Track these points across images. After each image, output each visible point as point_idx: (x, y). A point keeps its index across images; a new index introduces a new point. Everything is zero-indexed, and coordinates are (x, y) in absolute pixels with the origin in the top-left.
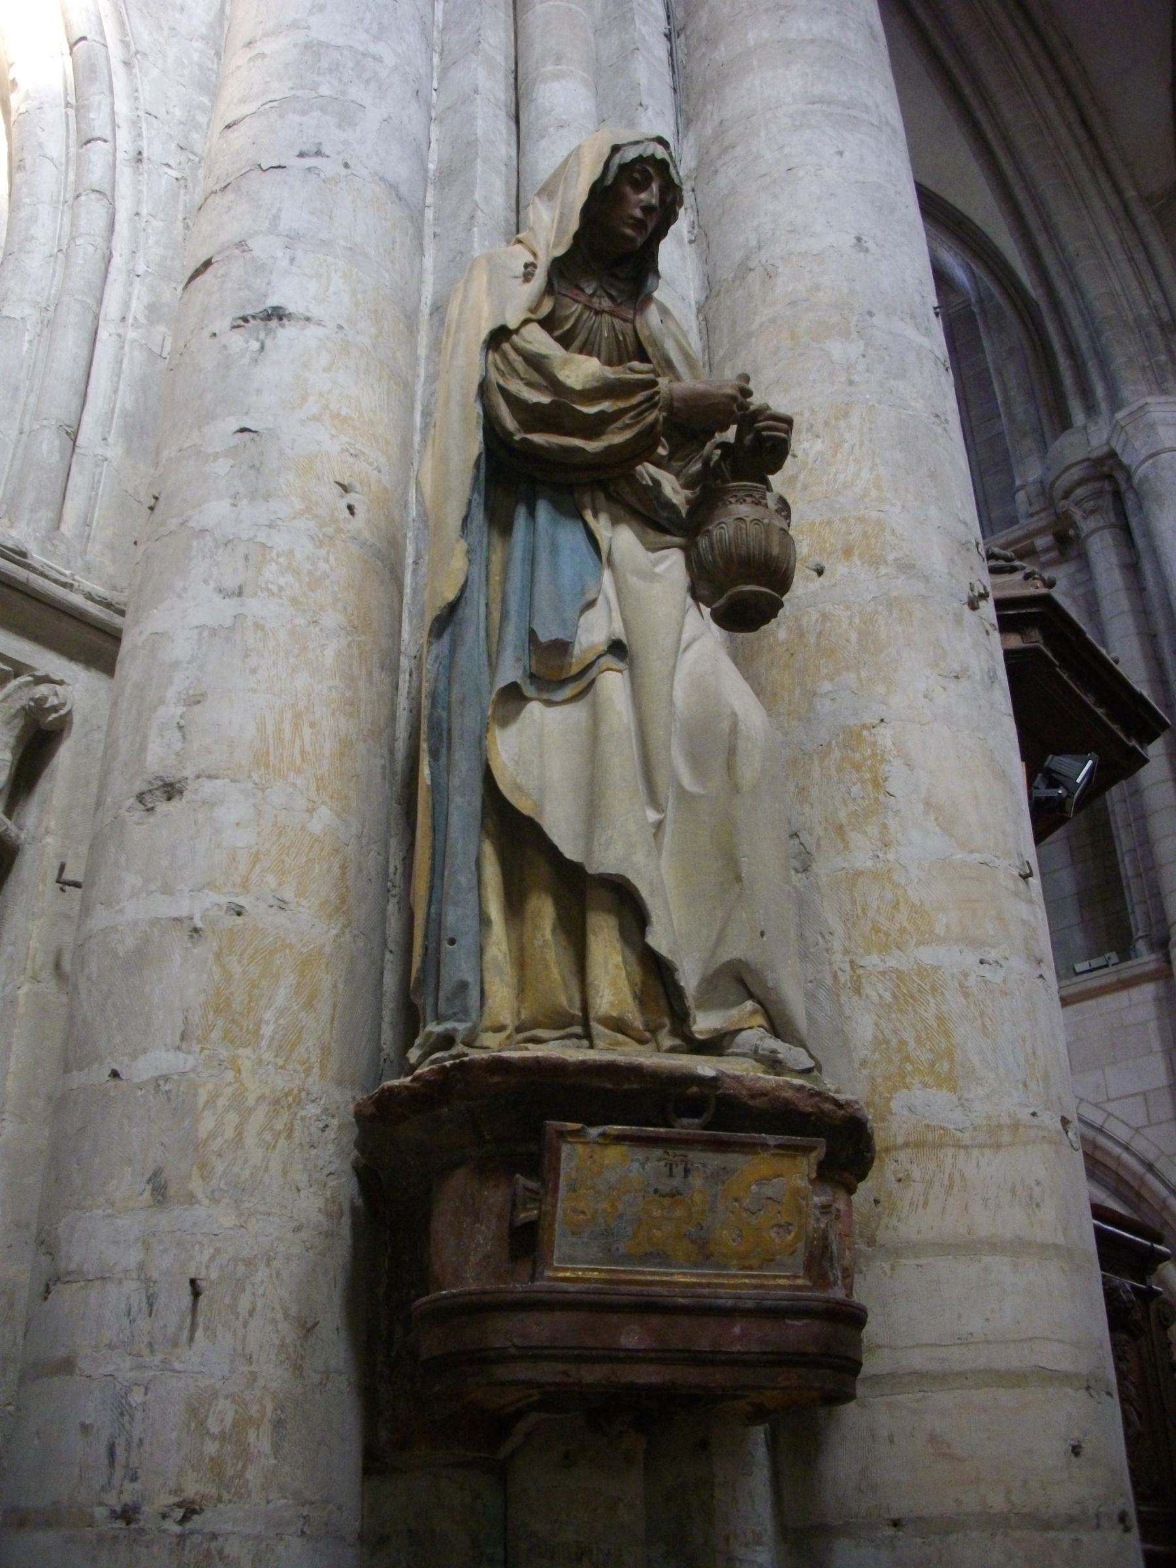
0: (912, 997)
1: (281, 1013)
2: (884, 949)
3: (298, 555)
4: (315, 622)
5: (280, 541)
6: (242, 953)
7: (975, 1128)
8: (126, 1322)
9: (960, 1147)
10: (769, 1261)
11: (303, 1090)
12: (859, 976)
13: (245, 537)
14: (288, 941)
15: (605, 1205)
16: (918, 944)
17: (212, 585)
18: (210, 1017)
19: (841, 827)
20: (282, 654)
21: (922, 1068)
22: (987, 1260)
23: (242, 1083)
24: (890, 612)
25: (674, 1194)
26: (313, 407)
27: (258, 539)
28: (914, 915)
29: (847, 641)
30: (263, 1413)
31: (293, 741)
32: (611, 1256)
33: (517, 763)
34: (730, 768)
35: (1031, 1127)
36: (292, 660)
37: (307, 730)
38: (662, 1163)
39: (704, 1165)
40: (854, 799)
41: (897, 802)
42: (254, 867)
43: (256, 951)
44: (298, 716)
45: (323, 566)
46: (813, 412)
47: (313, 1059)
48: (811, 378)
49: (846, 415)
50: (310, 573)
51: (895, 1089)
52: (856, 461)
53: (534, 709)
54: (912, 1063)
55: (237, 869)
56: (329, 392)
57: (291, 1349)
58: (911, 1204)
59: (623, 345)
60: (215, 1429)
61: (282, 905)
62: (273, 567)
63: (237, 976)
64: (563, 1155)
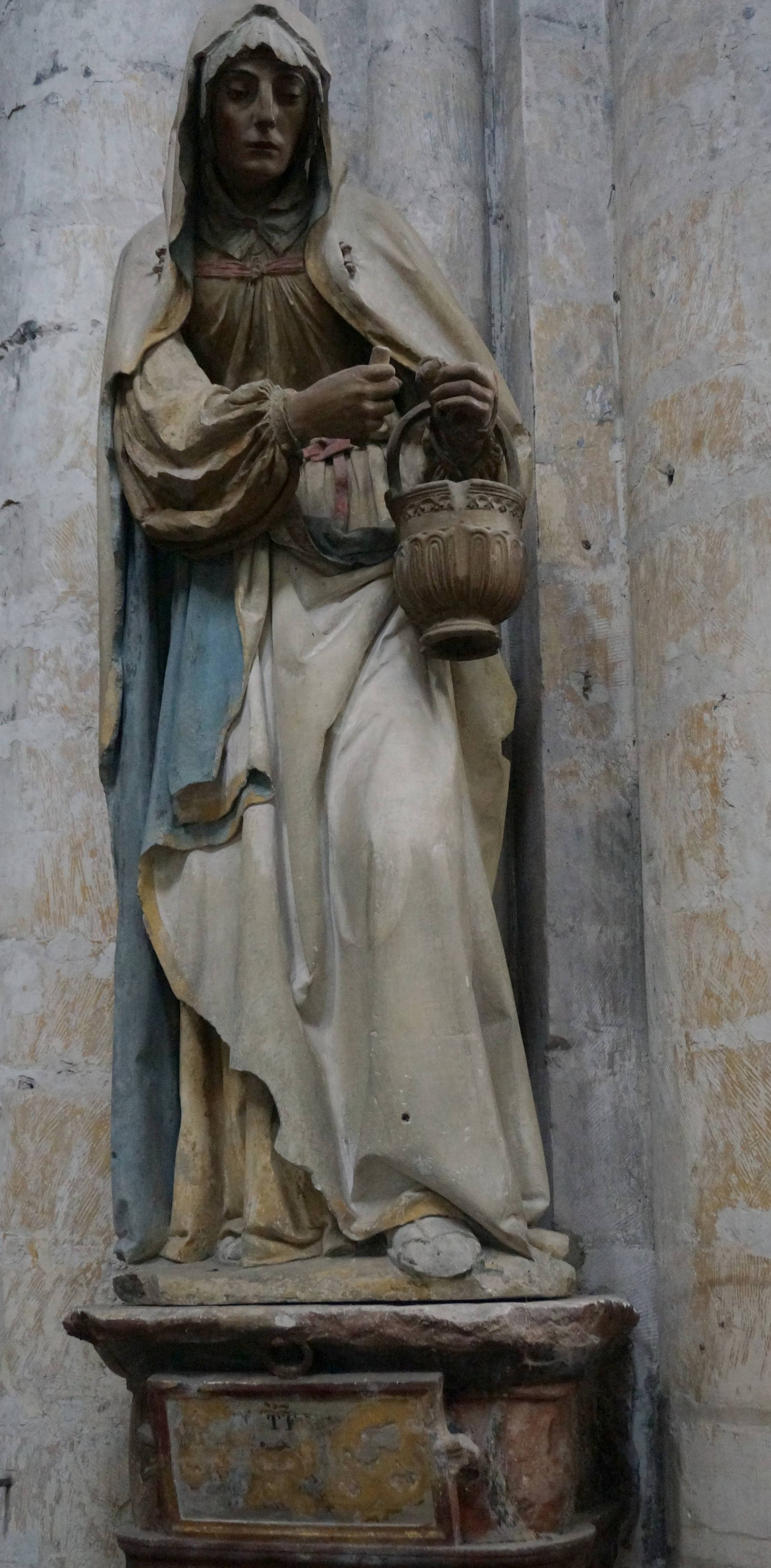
1: (75, 1185)
2: (715, 1020)
3: (65, 651)
4: (89, 728)
5: (45, 640)
6: (35, 1127)
10: (393, 1512)
11: (103, 1261)
12: (692, 1055)
13: (14, 643)
14: (78, 1106)
16: (750, 1014)
18: (11, 1200)
20: (56, 779)
21: (747, 1181)
23: (40, 1269)
24: (742, 526)
25: (281, 1447)
27: (26, 645)
28: (748, 973)
29: (693, 581)
31: (73, 880)
32: (231, 1510)
36: (66, 783)
38: (264, 1415)
39: (307, 1416)
40: (693, 813)
42: (40, 1033)
43: (47, 1125)
44: (76, 847)
46: (670, 217)
49: (705, 213)
50: (79, 669)
51: (719, 1207)
53: (195, 859)
55: (25, 1038)
58: (731, 1357)
61: (70, 1068)
62: (41, 675)
63: (31, 1155)
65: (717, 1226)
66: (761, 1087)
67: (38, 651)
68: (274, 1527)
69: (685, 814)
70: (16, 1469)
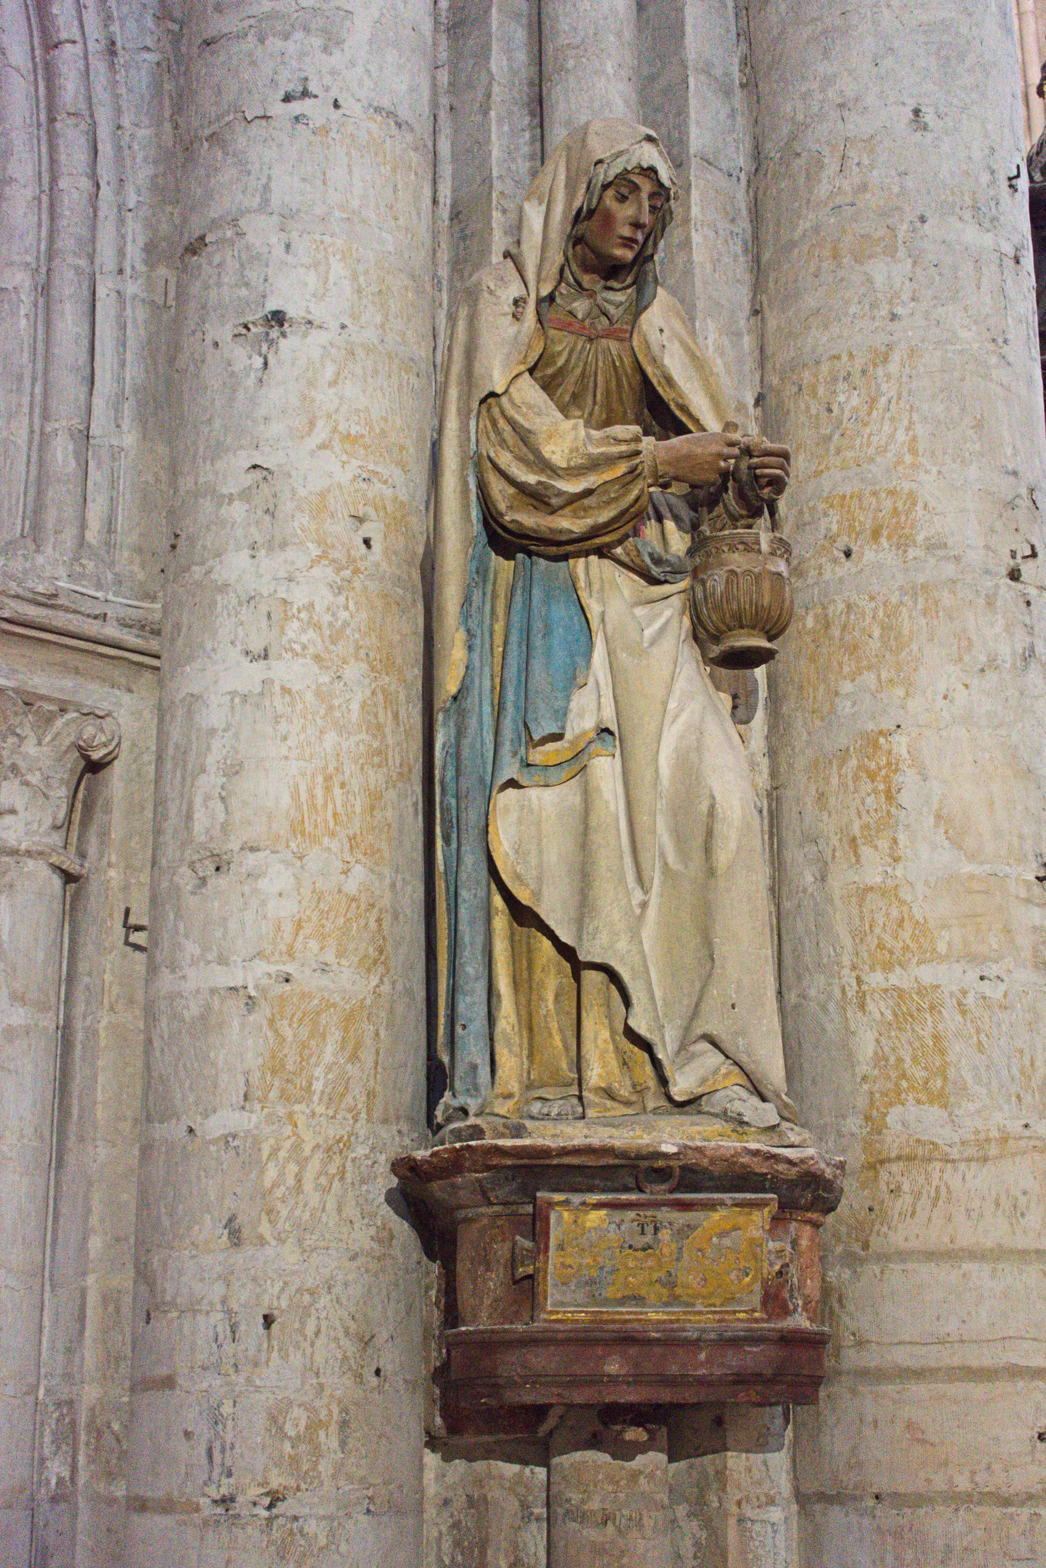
0: (912, 1016)
1: (329, 1069)
2: (887, 967)
3: (317, 607)
5: (299, 596)
6: (293, 1016)
7: (963, 1143)
8: (214, 1346)
9: (947, 1161)
12: (864, 993)
15: (588, 1260)
16: (919, 963)
17: (239, 648)
18: (268, 1077)
19: (854, 840)
20: (310, 717)
22: (967, 1266)
24: (916, 603)
26: (321, 434)
30: (330, 1414)
31: (326, 805)
33: (517, 852)
34: (708, 850)
35: (1021, 1138)
37: (337, 791)
41: (908, 816)
44: (328, 778)
45: (344, 615)
46: (851, 355)
47: (360, 1106)
48: (851, 311)
49: (886, 360)
50: (330, 624)
51: (891, 1104)
52: (892, 419)
54: (908, 1080)
56: (337, 411)
57: (352, 1361)
59: (620, 371)
60: (291, 1432)
61: (324, 969)
62: (295, 624)
64: (552, 1221)
65: (888, 1119)
66: (928, 1016)
67: (291, 603)
68: (631, 1313)
69: (859, 812)
70: (279, 1308)
